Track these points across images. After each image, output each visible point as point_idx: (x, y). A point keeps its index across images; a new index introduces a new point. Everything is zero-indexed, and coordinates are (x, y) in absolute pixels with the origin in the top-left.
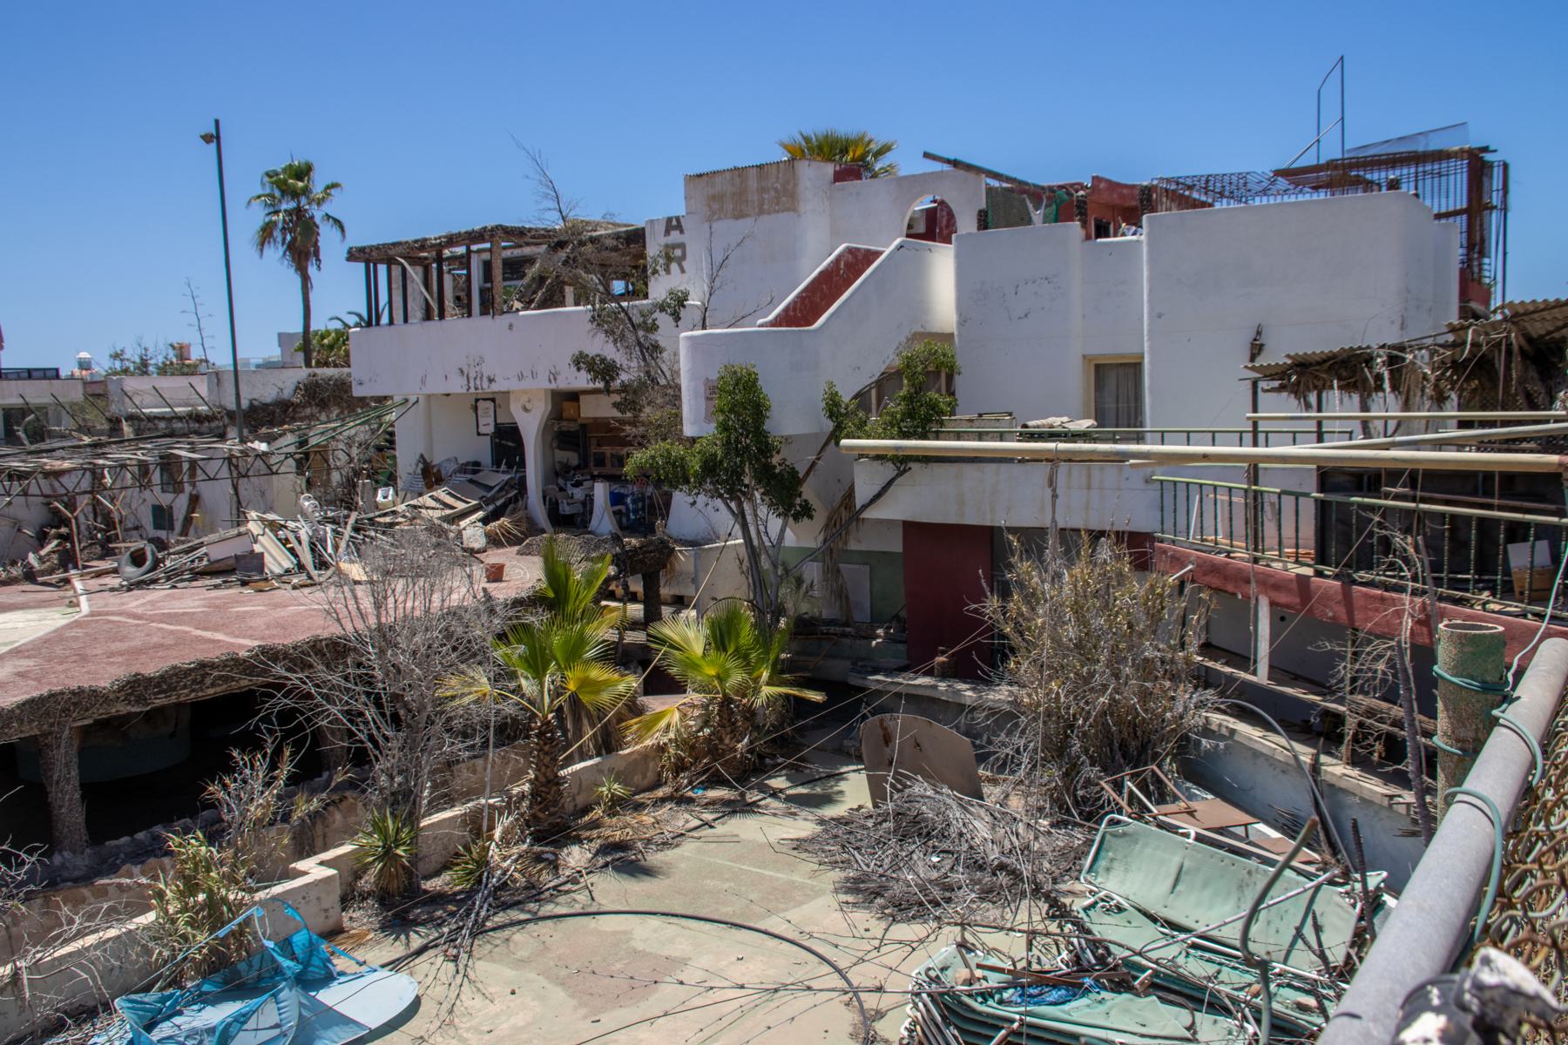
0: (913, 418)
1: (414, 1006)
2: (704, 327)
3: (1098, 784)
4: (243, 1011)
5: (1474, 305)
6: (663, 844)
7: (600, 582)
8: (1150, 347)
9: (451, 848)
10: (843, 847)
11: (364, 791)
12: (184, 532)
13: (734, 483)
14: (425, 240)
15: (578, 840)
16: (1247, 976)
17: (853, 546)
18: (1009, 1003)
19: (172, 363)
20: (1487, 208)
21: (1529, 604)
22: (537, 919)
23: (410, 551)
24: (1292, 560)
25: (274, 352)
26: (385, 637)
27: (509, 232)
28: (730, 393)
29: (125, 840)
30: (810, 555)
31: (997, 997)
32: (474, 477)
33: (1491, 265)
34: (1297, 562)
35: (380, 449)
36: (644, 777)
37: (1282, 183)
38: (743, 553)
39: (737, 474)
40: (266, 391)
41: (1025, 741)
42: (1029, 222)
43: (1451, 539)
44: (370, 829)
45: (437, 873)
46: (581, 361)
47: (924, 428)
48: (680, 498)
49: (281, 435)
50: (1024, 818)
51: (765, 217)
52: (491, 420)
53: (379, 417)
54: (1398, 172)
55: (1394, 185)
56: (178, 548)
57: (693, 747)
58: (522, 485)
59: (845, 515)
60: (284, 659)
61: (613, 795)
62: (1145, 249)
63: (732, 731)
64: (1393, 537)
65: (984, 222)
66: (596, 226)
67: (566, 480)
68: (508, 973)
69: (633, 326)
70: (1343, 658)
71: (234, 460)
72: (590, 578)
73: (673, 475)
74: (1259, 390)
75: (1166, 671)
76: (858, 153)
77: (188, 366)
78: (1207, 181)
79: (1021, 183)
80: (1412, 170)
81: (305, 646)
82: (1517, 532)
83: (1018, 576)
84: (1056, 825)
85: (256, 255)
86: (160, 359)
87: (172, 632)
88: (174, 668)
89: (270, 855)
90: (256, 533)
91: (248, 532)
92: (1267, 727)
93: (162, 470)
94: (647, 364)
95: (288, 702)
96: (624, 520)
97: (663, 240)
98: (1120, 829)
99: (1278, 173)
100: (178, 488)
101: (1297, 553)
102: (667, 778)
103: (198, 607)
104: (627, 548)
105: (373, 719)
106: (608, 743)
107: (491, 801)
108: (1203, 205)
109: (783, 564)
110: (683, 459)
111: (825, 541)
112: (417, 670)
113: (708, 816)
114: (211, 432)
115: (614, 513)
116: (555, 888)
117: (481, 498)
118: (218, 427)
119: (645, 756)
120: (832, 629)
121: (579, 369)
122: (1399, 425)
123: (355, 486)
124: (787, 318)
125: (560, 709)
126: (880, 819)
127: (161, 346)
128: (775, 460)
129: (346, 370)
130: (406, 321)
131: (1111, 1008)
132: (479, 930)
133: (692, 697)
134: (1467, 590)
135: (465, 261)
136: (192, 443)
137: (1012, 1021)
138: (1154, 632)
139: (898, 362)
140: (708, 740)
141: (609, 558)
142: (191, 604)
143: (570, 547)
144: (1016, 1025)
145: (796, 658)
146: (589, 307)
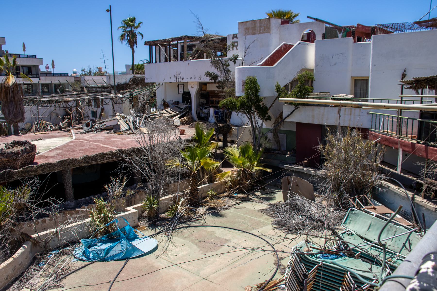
0: (301, 93)
1: (157, 247)
2: (242, 65)
3: (348, 199)
6: (225, 208)
7: (211, 136)
8: (372, 75)
9: (168, 206)
10: (275, 212)
11: (145, 190)
12: (100, 118)
14: (166, 39)
15: (202, 206)
17: (282, 129)
18: (319, 258)
19: (97, 72)
22: (190, 226)
24: (410, 138)
25: (124, 70)
26: (152, 148)
27: (189, 38)
30: (270, 130)
31: (315, 256)
34: (411, 139)
35: (152, 97)
36: (221, 190)
37: (416, 26)
38: (251, 129)
39: (250, 107)
40: (122, 80)
41: (328, 186)
42: (337, 37)
44: (146, 200)
45: (164, 213)
46: (208, 74)
47: (304, 96)
48: (234, 113)
49: (126, 93)
50: (326, 207)
52: (182, 90)
53: (152, 88)
56: (98, 122)
57: (235, 182)
58: (190, 108)
59: (280, 120)
61: (212, 194)
62: (372, 45)
63: (246, 179)
65: (324, 37)
66: (213, 36)
67: (203, 107)
68: (181, 240)
70: (424, 167)
71: (113, 99)
72: (208, 135)
73: (232, 107)
74: (404, 88)
75: (370, 168)
78: (392, 25)
79: (336, 25)
81: (131, 150)
84: (335, 210)
86: (94, 71)
87: (96, 145)
88: (96, 154)
89: (120, 205)
91: (116, 119)
92: (399, 186)
94: (226, 76)
96: (218, 119)
97: (232, 41)
98: (354, 212)
99: (415, 23)
100: (98, 107)
101: (412, 136)
102: (227, 191)
104: (219, 127)
106: (211, 180)
107: (179, 194)
108: (391, 32)
109: (262, 133)
110: (235, 102)
111: (274, 127)
112: (160, 158)
113: (238, 202)
114: (107, 92)
115: (216, 117)
116: (195, 218)
118: (109, 90)
119: (221, 184)
120: (275, 152)
121: (207, 76)
123: (145, 107)
124: (266, 63)
125: (198, 170)
126: (286, 205)
128: (261, 104)
130: (160, 62)
131: (348, 262)
132: (174, 229)
133: (235, 168)
135: (176, 46)
136: (102, 94)
137: (319, 263)
138: (367, 157)
140: (239, 181)
141: (214, 129)
143: (203, 126)
144: (320, 264)
146: (211, 59)
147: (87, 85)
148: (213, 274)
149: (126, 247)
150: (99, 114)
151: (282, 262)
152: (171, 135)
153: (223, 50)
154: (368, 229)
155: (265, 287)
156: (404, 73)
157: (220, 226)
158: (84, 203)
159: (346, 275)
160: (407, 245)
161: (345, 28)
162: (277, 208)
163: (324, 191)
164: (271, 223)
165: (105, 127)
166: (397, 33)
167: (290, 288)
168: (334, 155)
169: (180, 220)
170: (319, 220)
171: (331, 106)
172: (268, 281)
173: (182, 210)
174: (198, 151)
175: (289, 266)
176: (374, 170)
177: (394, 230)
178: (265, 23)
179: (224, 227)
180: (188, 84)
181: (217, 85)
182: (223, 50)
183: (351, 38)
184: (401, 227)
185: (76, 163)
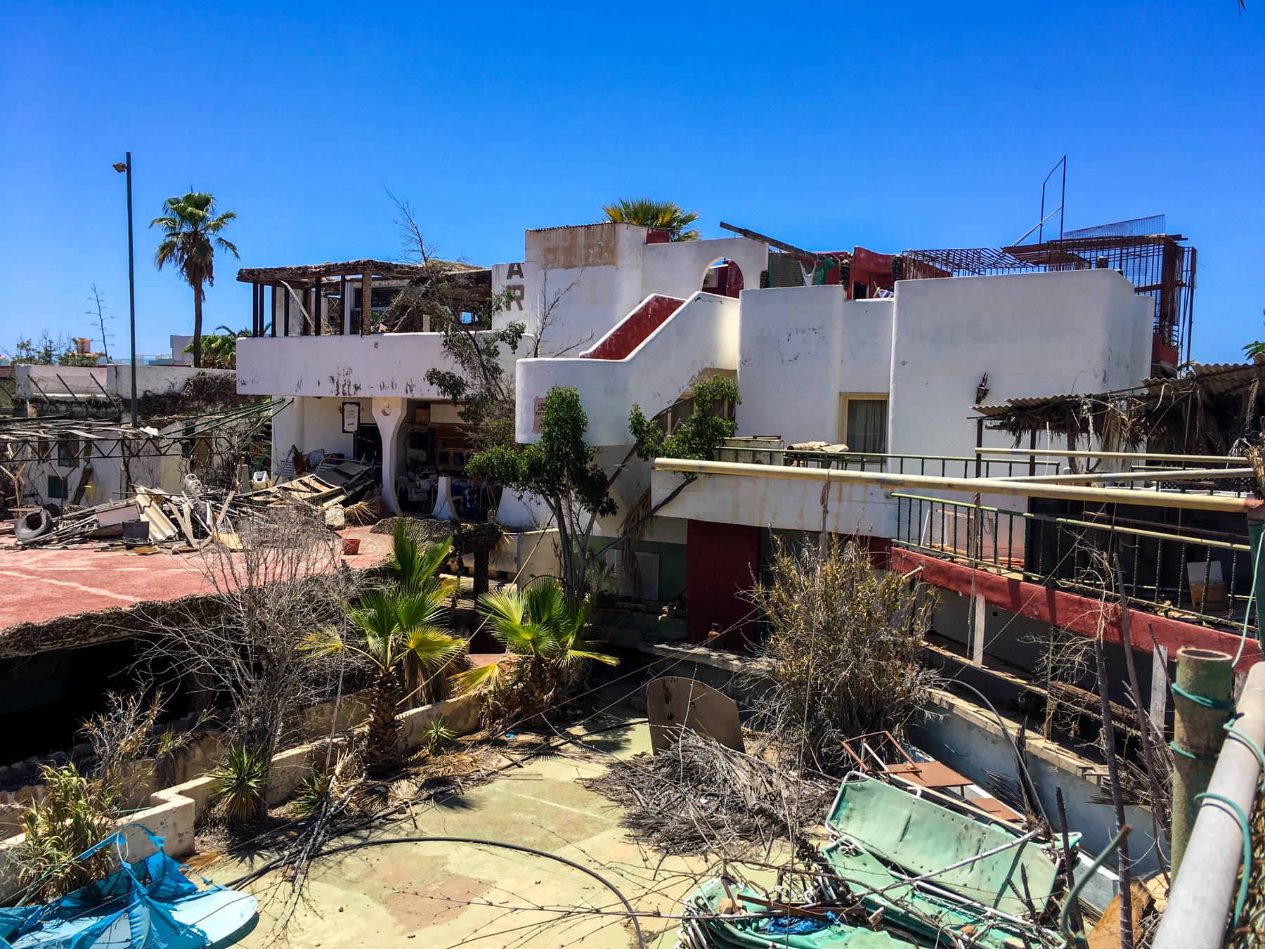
0: (701, 438)
2: (536, 356)
3: (839, 744)
4: (98, 926)
5: (1163, 364)
6: (479, 780)
8: (895, 388)
9: (296, 781)
10: (628, 787)
11: (224, 730)
12: (76, 501)
13: (554, 483)
14: (307, 268)
15: (407, 776)
16: (963, 917)
17: (647, 538)
18: (763, 931)
19: (73, 355)
20: (1178, 285)
21: (1204, 613)
22: (366, 844)
23: (282, 526)
24: (1005, 566)
25: (167, 353)
26: (255, 597)
28: (556, 410)
30: (610, 543)
31: (754, 925)
32: (338, 467)
33: (1179, 331)
34: (1009, 568)
35: (255, 438)
36: (466, 722)
37: (1010, 258)
39: (557, 475)
40: (159, 383)
41: (776, 705)
42: (802, 283)
43: (1140, 556)
44: (227, 763)
45: (283, 803)
46: (434, 377)
47: (709, 446)
48: (509, 494)
49: (170, 423)
50: (777, 769)
51: (589, 268)
52: (355, 421)
53: (259, 412)
54: (1106, 253)
55: (1103, 264)
56: (70, 514)
57: (508, 698)
58: (379, 471)
59: (642, 513)
61: (439, 736)
62: (895, 308)
63: (542, 686)
64: (1092, 552)
65: (766, 281)
67: (415, 472)
70: (1047, 651)
71: (127, 442)
72: (432, 555)
73: (507, 474)
74: (984, 427)
75: (898, 652)
76: (667, 219)
78: (948, 254)
79: (797, 250)
80: (1118, 252)
81: (183, 604)
84: (804, 776)
85: (155, 269)
86: (63, 351)
87: (61, 587)
88: (62, 619)
90: (142, 505)
92: (982, 704)
93: (59, 446)
94: (488, 382)
95: (166, 652)
96: (462, 508)
97: (506, 282)
98: (859, 784)
100: (74, 463)
101: (1010, 561)
102: (485, 724)
103: (87, 566)
105: (238, 667)
106: (438, 692)
107: (335, 740)
109: (591, 550)
110: (514, 461)
111: (625, 533)
112: (281, 627)
113: (517, 757)
114: (108, 417)
115: (454, 501)
116: (384, 817)
118: (114, 413)
119: (468, 705)
120: (627, 605)
121: (432, 384)
122: (1099, 461)
123: (234, 469)
126: (659, 765)
128: (589, 466)
129: (232, 371)
130: (286, 334)
131: (849, 940)
132: (315, 854)
133: (510, 656)
135: (339, 288)
136: (90, 425)
138: (889, 620)
139: (690, 391)
140: (521, 692)
141: (450, 539)
142: (81, 563)
143: (417, 530)
146: (443, 333)
150: (75, 488)
153: (480, 309)
154: (903, 835)
156: (981, 386)
160: (1017, 879)
161: (823, 259)
162: (634, 774)
163: (769, 721)
164: (618, 821)
168: (796, 615)
170: (762, 811)
173: (342, 790)
174: (401, 606)
176: (909, 657)
180: (373, 401)
182: (480, 309)
184: (994, 827)
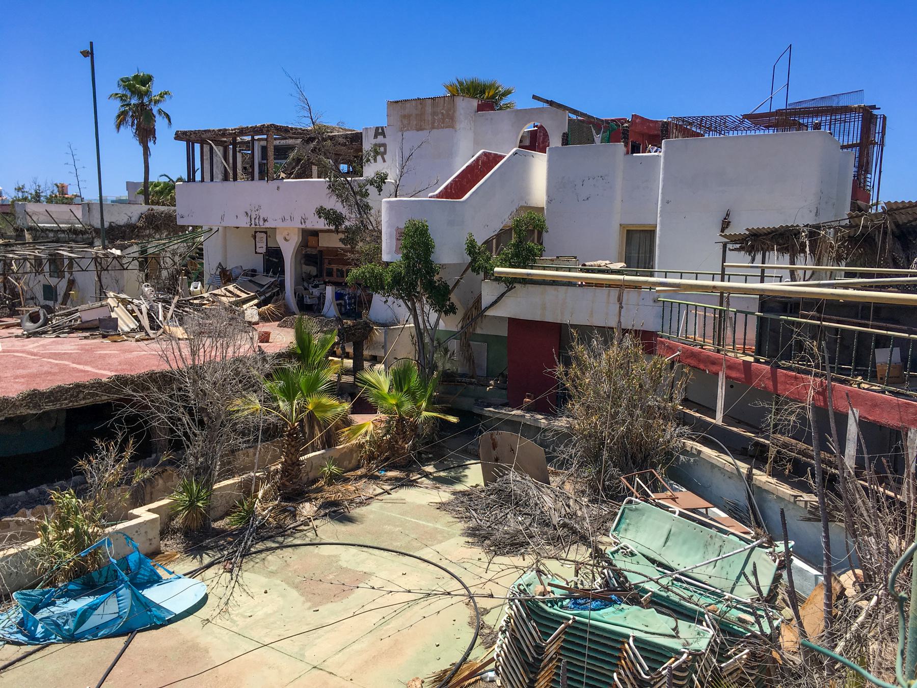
0: (518, 257)
1: (204, 600)
2: (396, 196)
4: (95, 602)
6: (361, 503)
7: (330, 346)
8: (661, 221)
11: (178, 467)
12: (64, 303)
14: (226, 130)
15: (310, 500)
16: (708, 599)
18: (566, 608)
19: (56, 196)
20: (872, 144)
22: (282, 547)
23: (215, 321)
24: (741, 352)
25: (124, 194)
26: (197, 372)
27: (278, 129)
28: (411, 236)
29: (21, 493)
30: (452, 335)
31: (559, 604)
33: (872, 178)
34: (744, 353)
37: (747, 123)
38: (414, 332)
39: (413, 285)
40: (120, 217)
42: (593, 141)
44: (182, 489)
45: (222, 518)
47: (524, 263)
49: (129, 246)
51: (435, 131)
52: (264, 245)
53: (193, 238)
54: (819, 119)
55: (817, 127)
56: (60, 312)
57: (379, 446)
58: (282, 285)
59: (475, 313)
60: (131, 384)
63: (403, 437)
65: (566, 140)
66: (333, 129)
67: (309, 283)
68: (263, 580)
69: (354, 192)
71: (99, 260)
72: (323, 343)
73: (376, 284)
74: (727, 249)
75: (661, 413)
77: (67, 198)
78: (702, 120)
79: (589, 117)
80: (828, 118)
82: (882, 342)
83: (576, 353)
85: (116, 130)
86: (49, 193)
87: (57, 364)
88: (59, 387)
89: (116, 504)
90: (112, 306)
91: (108, 305)
92: (721, 451)
94: (361, 217)
96: (343, 309)
97: (374, 141)
99: (746, 117)
101: (744, 348)
102: (364, 463)
104: (345, 326)
105: (187, 422)
106: (329, 442)
107: (257, 474)
108: (698, 135)
109: (438, 340)
110: (381, 275)
111: (462, 328)
112: (217, 394)
113: (387, 487)
116: (294, 528)
117: (256, 292)
118: (88, 238)
119: (351, 450)
121: (320, 217)
122: (813, 274)
123: (177, 280)
124: (446, 194)
125: (301, 421)
127: (49, 185)
128: (436, 278)
129: (173, 208)
130: (212, 180)
131: (627, 614)
132: (246, 554)
134: (849, 375)
135: (250, 145)
136: (71, 247)
137: (569, 619)
138: (655, 390)
139: (510, 223)
140: (389, 441)
141: (336, 332)
143: (312, 324)
144: (570, 622)
145: (442, 396)
146: (327, 179)
147: (31, 224)
148: (337, 654)
149: (130, 605)
150: (62, 294)
151: (489, 620)
152: (242, 344)
154: (666, 542)
155: (451, 678)
156: (725, 219)
157: (350, 542)
158: (23, 502)
159: (626, 645)
161: (609, 123)
165: (78, 322)
166: (718, 136)
167: (506, 678)
169: (259, 534)
171: (579, 285)
172: (457, 665)
174: (302, 380)
175: (504, 629)
177: (718, 543)
178: (444, 106)
179: (359, 546)
180: (277, 230)
181: (342, 236)
183: (621, 147)
184: (731, 537)
185: (4, 409)
